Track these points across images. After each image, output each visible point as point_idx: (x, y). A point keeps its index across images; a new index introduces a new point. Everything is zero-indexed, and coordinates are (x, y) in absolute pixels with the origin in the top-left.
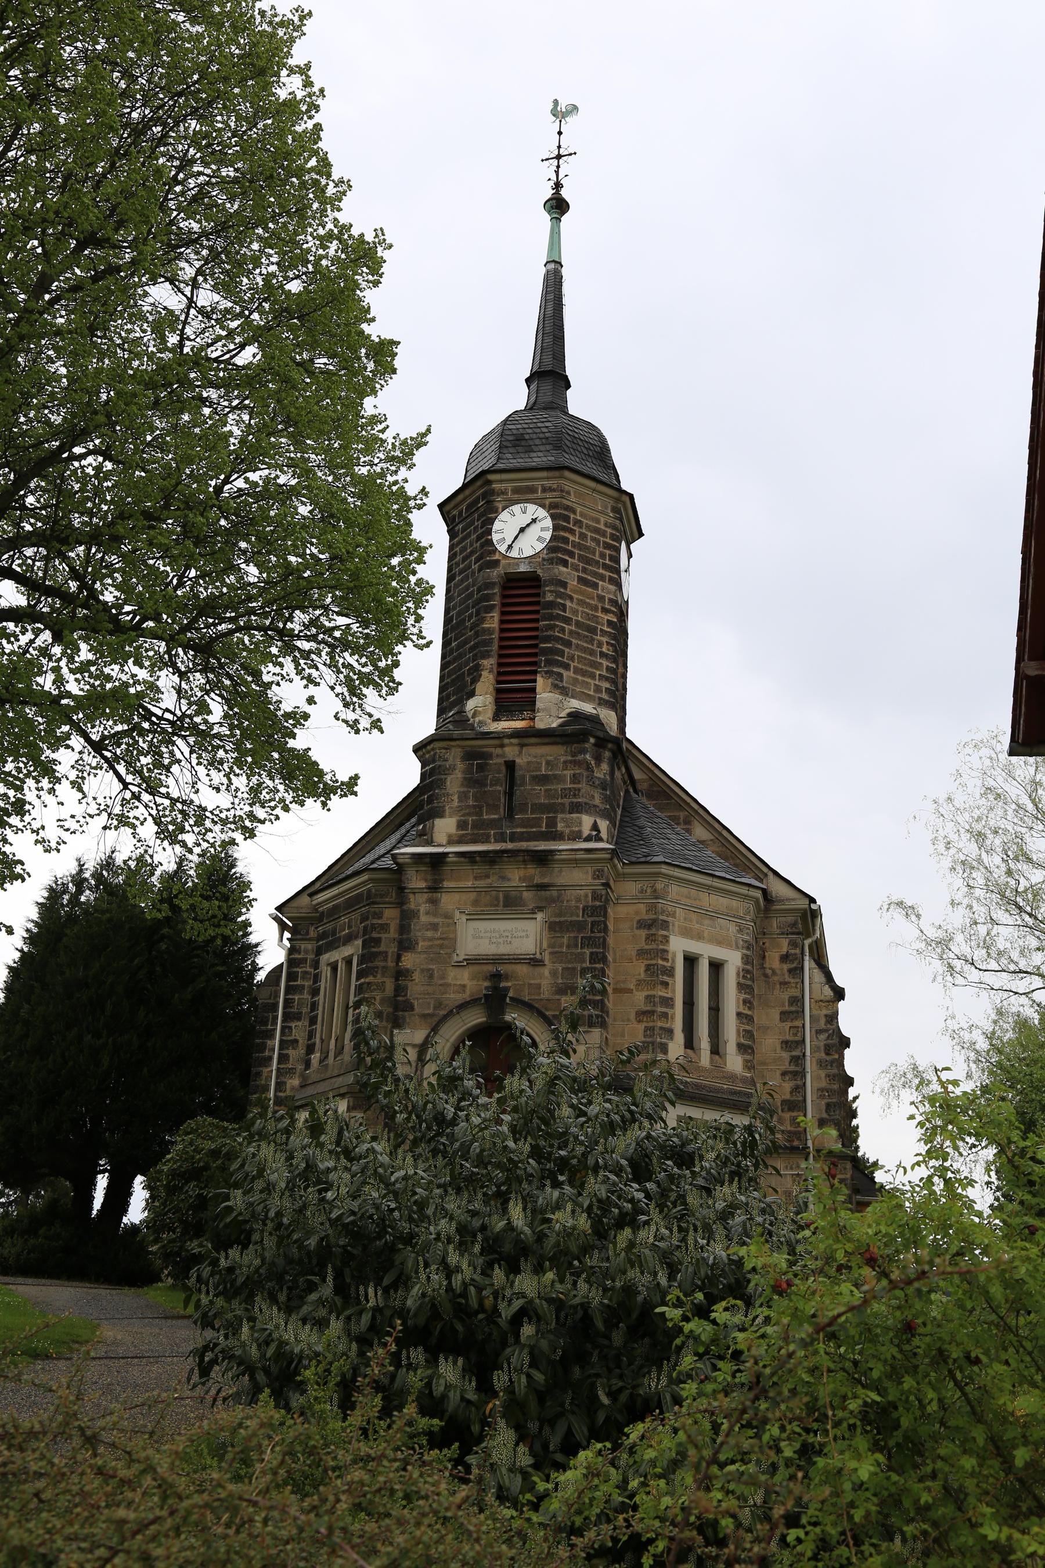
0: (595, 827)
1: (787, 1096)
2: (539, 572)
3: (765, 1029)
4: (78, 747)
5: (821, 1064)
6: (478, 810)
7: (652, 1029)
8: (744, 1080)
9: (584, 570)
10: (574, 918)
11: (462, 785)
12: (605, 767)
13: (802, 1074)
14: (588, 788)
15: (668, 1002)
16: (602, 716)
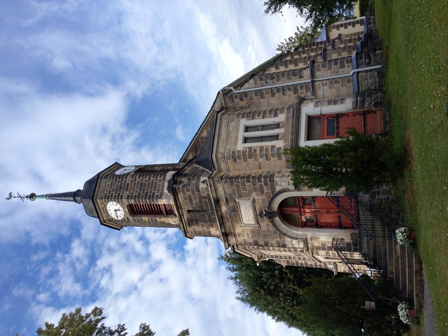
0: (203, 182)
1: (292, 92)
2: (126, 205)
3: (269, 105)
5: (278, 80)
6: (205, 221)
7: (272, 154)
8: (288, 113)
9: (123, 189)
10: (236, 189)
11: (199, 226)
12: (183, 179)
13: (283, 88)
14: (191, 186)
15: (261, 148)
16: (169, 179)
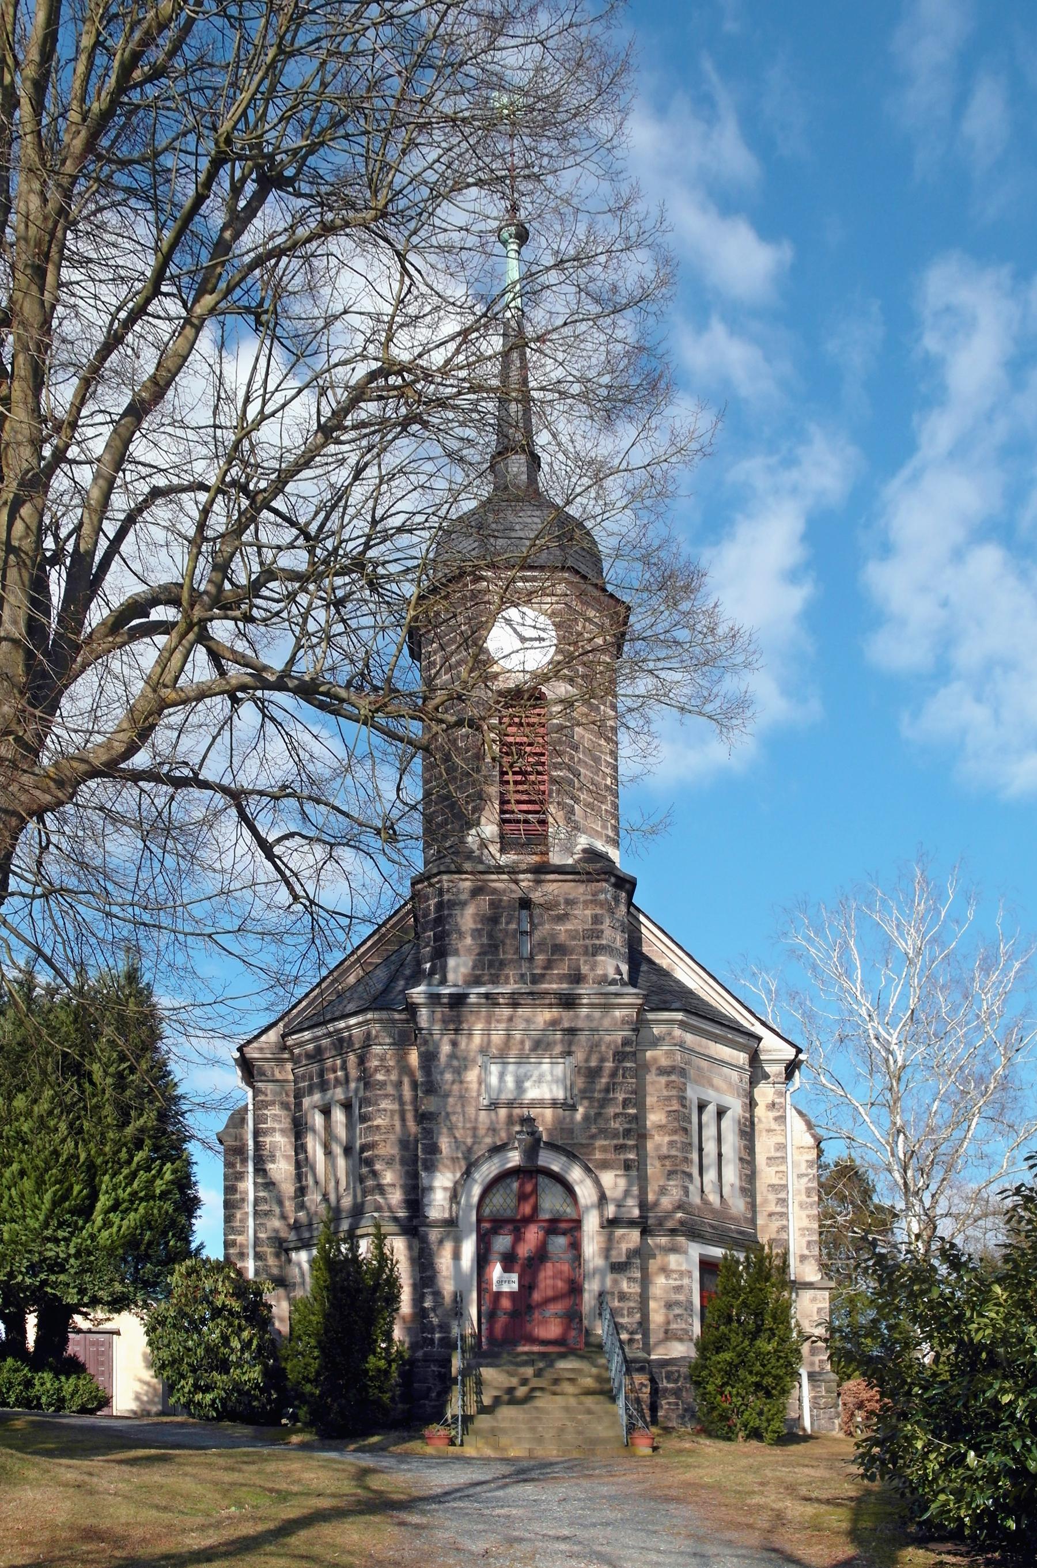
4: (284, 849)
